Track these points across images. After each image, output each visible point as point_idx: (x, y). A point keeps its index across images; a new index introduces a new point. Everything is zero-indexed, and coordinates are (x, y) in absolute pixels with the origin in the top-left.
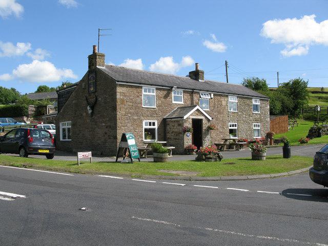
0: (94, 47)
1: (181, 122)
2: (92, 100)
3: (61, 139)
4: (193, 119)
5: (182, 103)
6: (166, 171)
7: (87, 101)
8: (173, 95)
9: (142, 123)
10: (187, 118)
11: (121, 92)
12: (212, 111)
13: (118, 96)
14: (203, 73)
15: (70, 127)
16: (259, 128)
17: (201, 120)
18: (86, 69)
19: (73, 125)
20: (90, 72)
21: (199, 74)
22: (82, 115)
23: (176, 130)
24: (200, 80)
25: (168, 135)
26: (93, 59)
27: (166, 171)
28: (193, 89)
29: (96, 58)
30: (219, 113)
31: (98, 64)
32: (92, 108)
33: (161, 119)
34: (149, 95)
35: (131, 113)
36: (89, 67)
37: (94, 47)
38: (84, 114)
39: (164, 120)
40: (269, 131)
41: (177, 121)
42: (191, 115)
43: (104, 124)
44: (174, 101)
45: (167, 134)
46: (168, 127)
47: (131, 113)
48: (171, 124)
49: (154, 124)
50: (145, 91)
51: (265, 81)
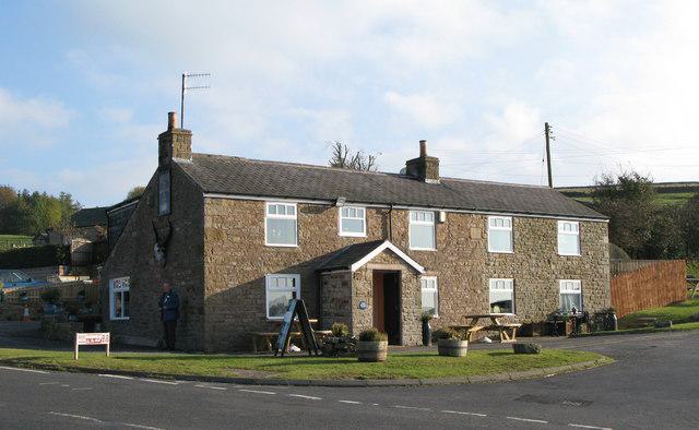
0: (171, 115)
1: (346, 278)
2: (164, 231)
4: (376, 273)
5: (364, 235)
6: (539, 372)
7: (157, 234)
8: (341, 218)
10: (360, 269)
11: (216, 210)
13: (208, 224)
14: (435, 162)
15: (127, 289)
17: (398, 273)
18: (154, 165)
19: (133, 284)
20: (160, 170)
21: (424, 167)
22: (147, 264)
23: (339, 296)
24: (428, 181)
25: (326, 307)
26: (165, 140)
27: (539, 372)
28: (390, 204)
29: (171, 142)
30: (462, 256)
31: (175, 152)
34: (280, 221)
36: (161, 159)
37: (171, 115)
38: (152, 261)
42: (373, 261)
43: (183, 283)
44: (344, 230)
45: (324, 305)
48: (332, 282)
50: (273, 210)
51: (68, 197)
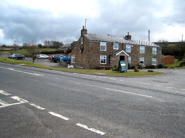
2: (82, 48)
3: (72, 63)
4: (120, 56)
8: (114, 46)
9: (100, 56)
10: (118, 55)
12: (132, 52)
16: (156, 61)
17: (124, 56)
32: (82, 50)
33: (108, 55)
35: (95, 53)
39: (110, 56)
40: (132, 39)
41: (114, 56)
42: (120, 54)
46: (111, 59)
47: (95, 53)
49: (105, 57)
50: (141, 48)
